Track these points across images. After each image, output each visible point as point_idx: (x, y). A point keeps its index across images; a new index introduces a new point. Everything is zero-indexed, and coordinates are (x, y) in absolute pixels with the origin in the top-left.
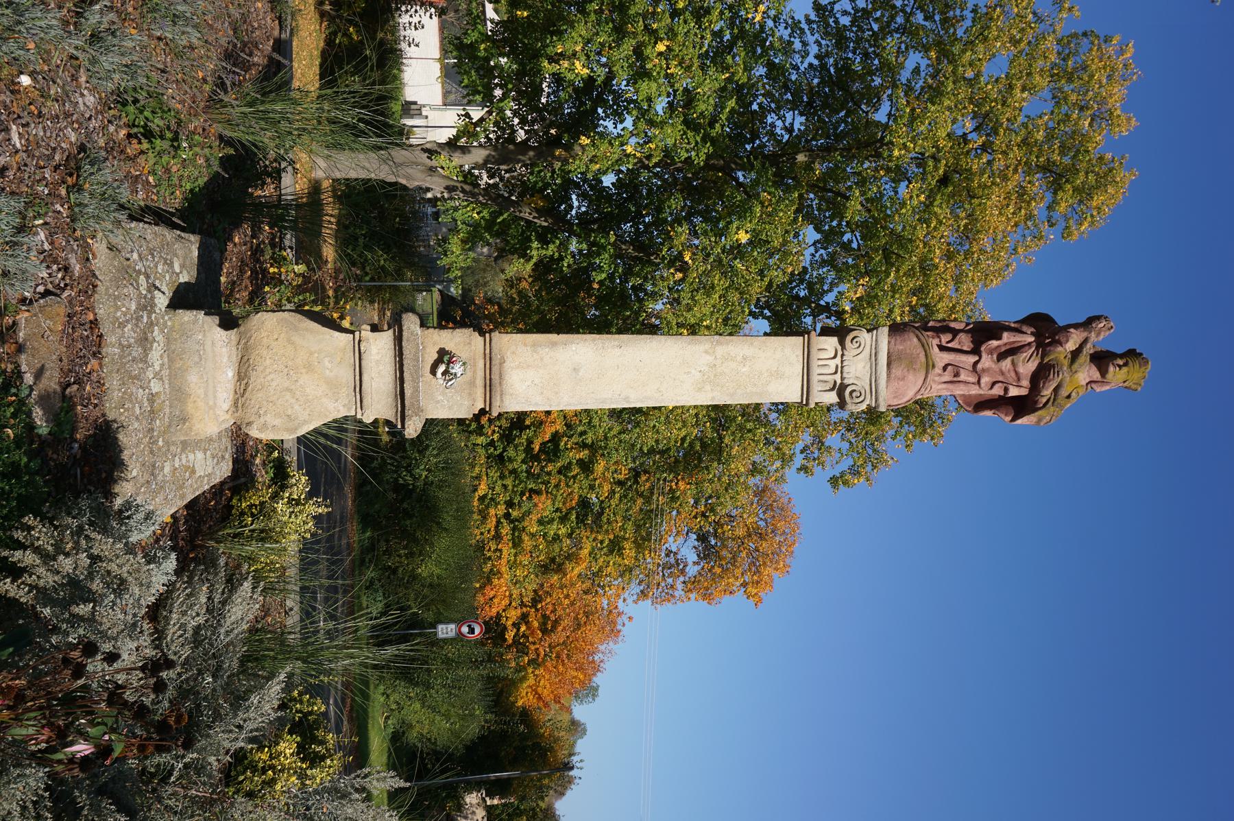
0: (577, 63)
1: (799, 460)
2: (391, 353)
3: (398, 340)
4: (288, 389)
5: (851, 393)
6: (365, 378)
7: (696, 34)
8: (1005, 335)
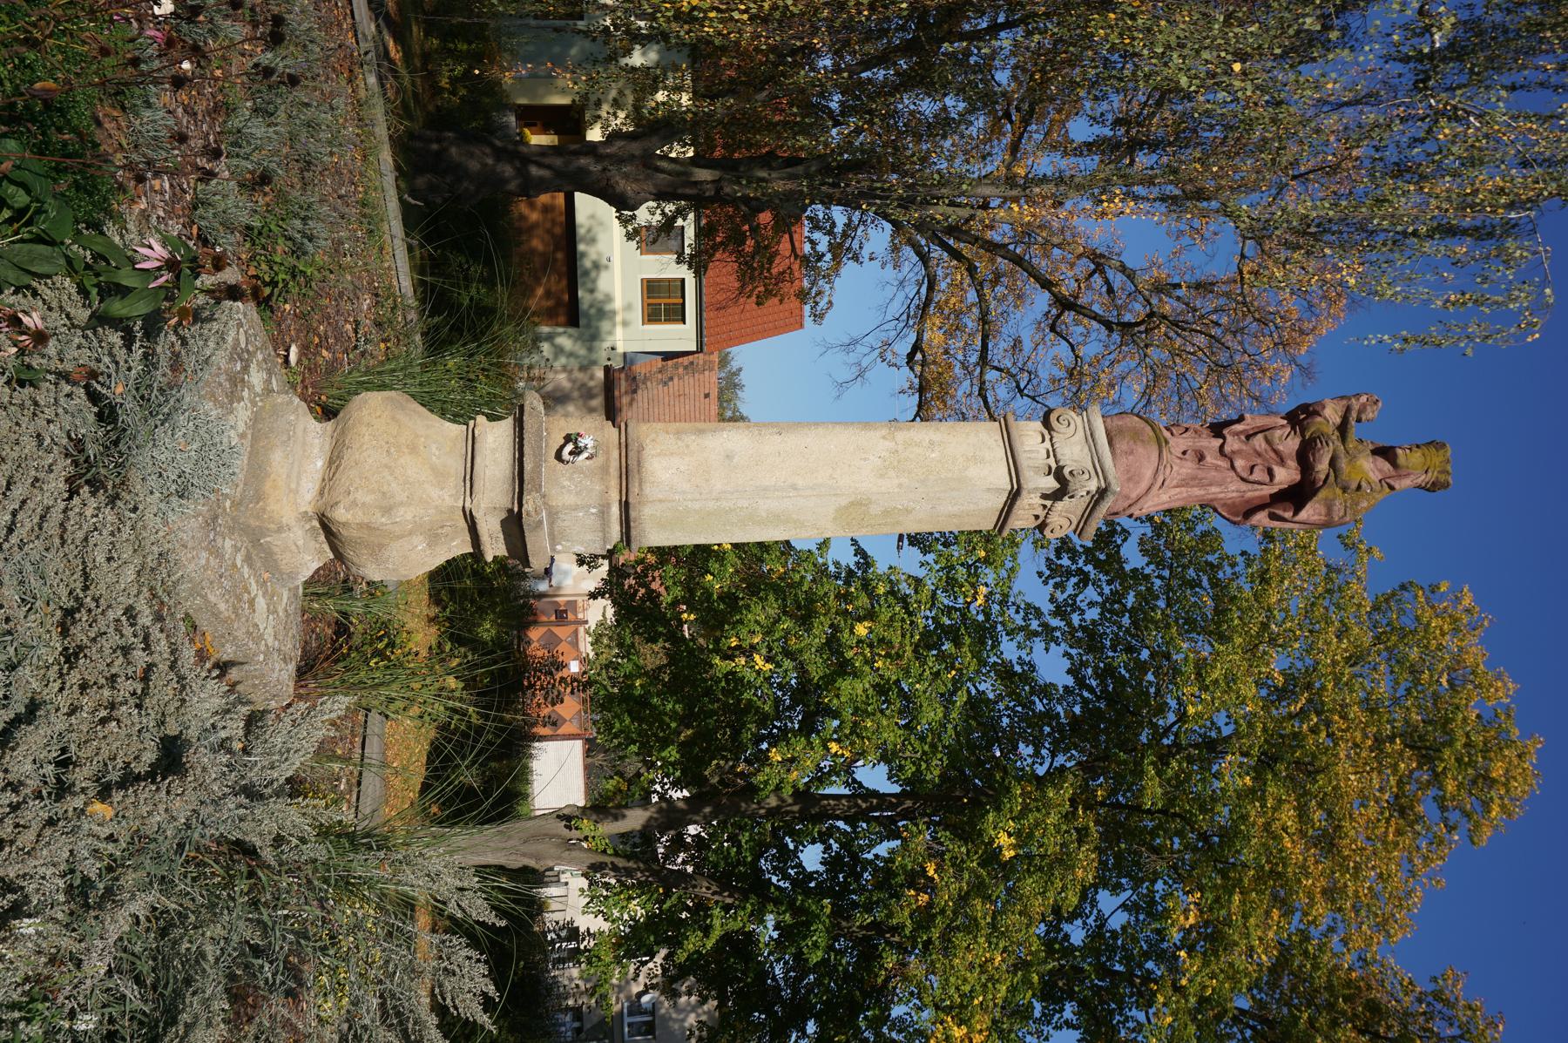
0: (757, 657)
2: (511, 439)
3: (519, 424)
4: (386, 466)
6: (478, 460)
7: (903, 620)
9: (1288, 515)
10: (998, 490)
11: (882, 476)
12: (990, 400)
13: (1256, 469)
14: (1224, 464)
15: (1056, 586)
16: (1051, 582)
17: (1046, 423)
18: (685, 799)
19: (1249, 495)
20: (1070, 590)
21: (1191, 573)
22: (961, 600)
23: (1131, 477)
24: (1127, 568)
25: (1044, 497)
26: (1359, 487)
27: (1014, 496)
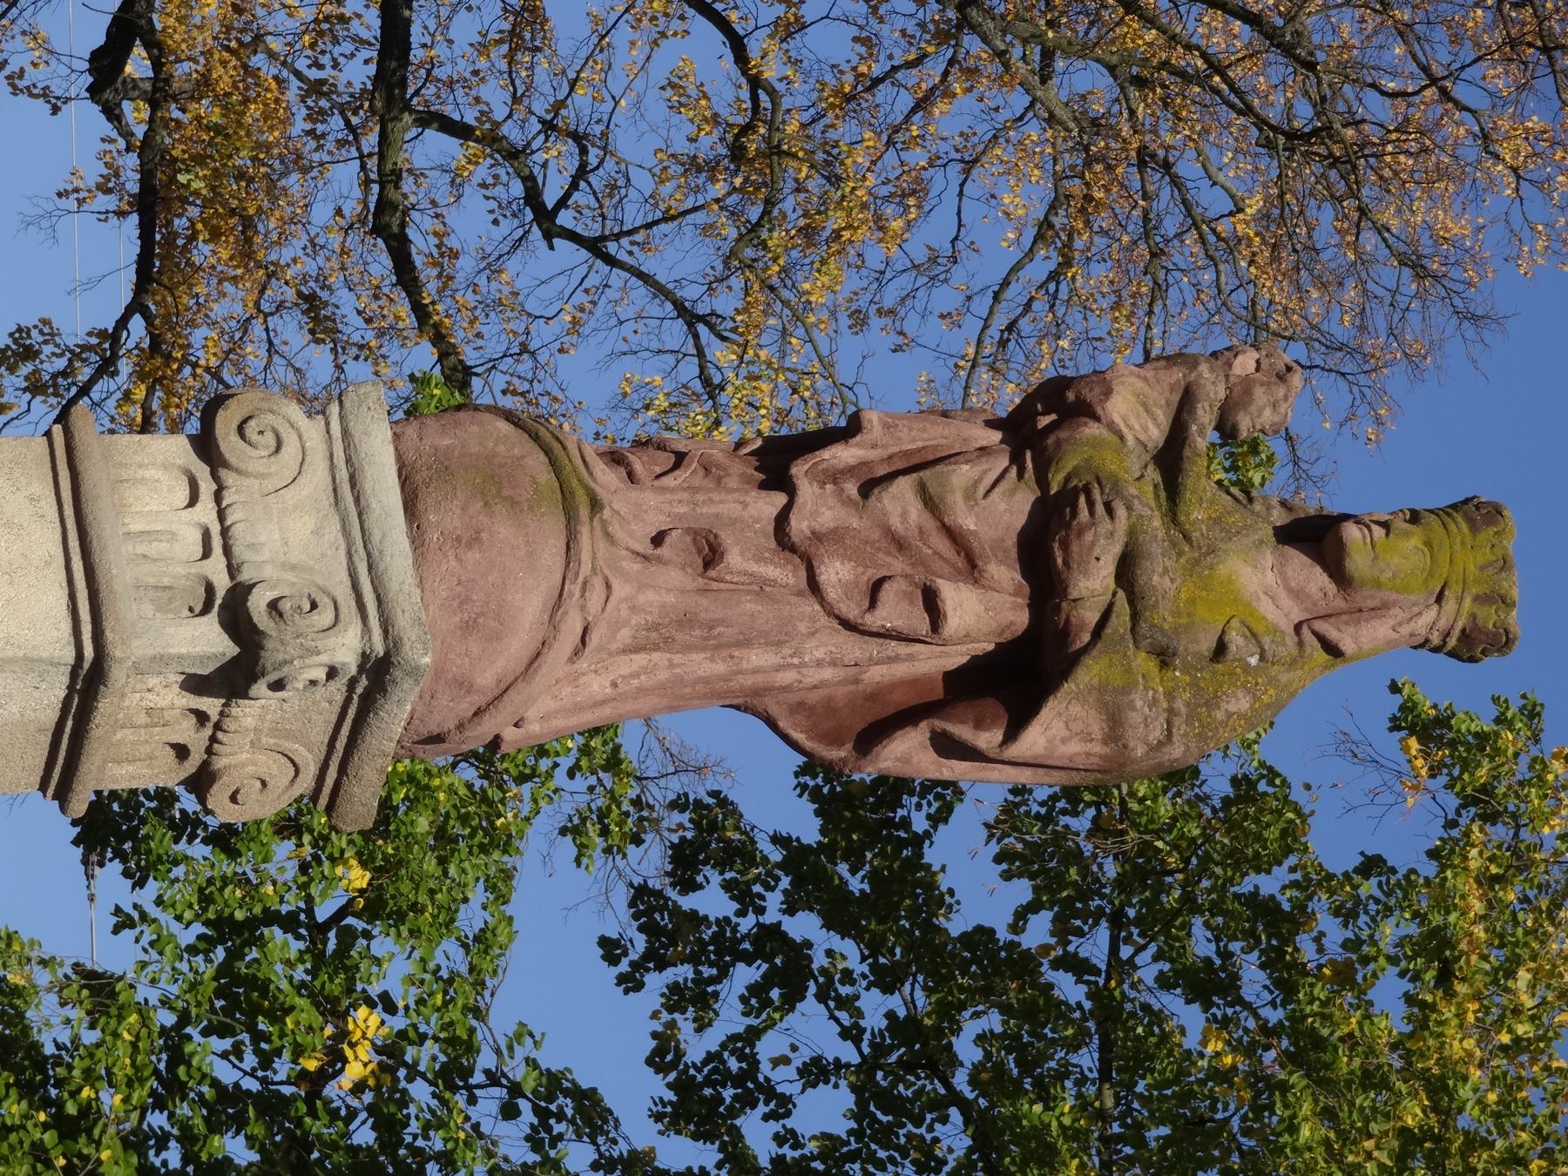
9: (988, 739)
10: (31, 663)
12: (421, 244)
13: (888, 593)
14: (786, 574)
15: (677, 998)
16: (656, 982)
17: (205, 446)
19: (877, 674)
20: (730, 1018)
21: (1201, 945)
22: (283, 1068)
23: (476, 620)
24: (956, 926)
25: (195, 684)
26: (1220, 649)
27: (88, 682)
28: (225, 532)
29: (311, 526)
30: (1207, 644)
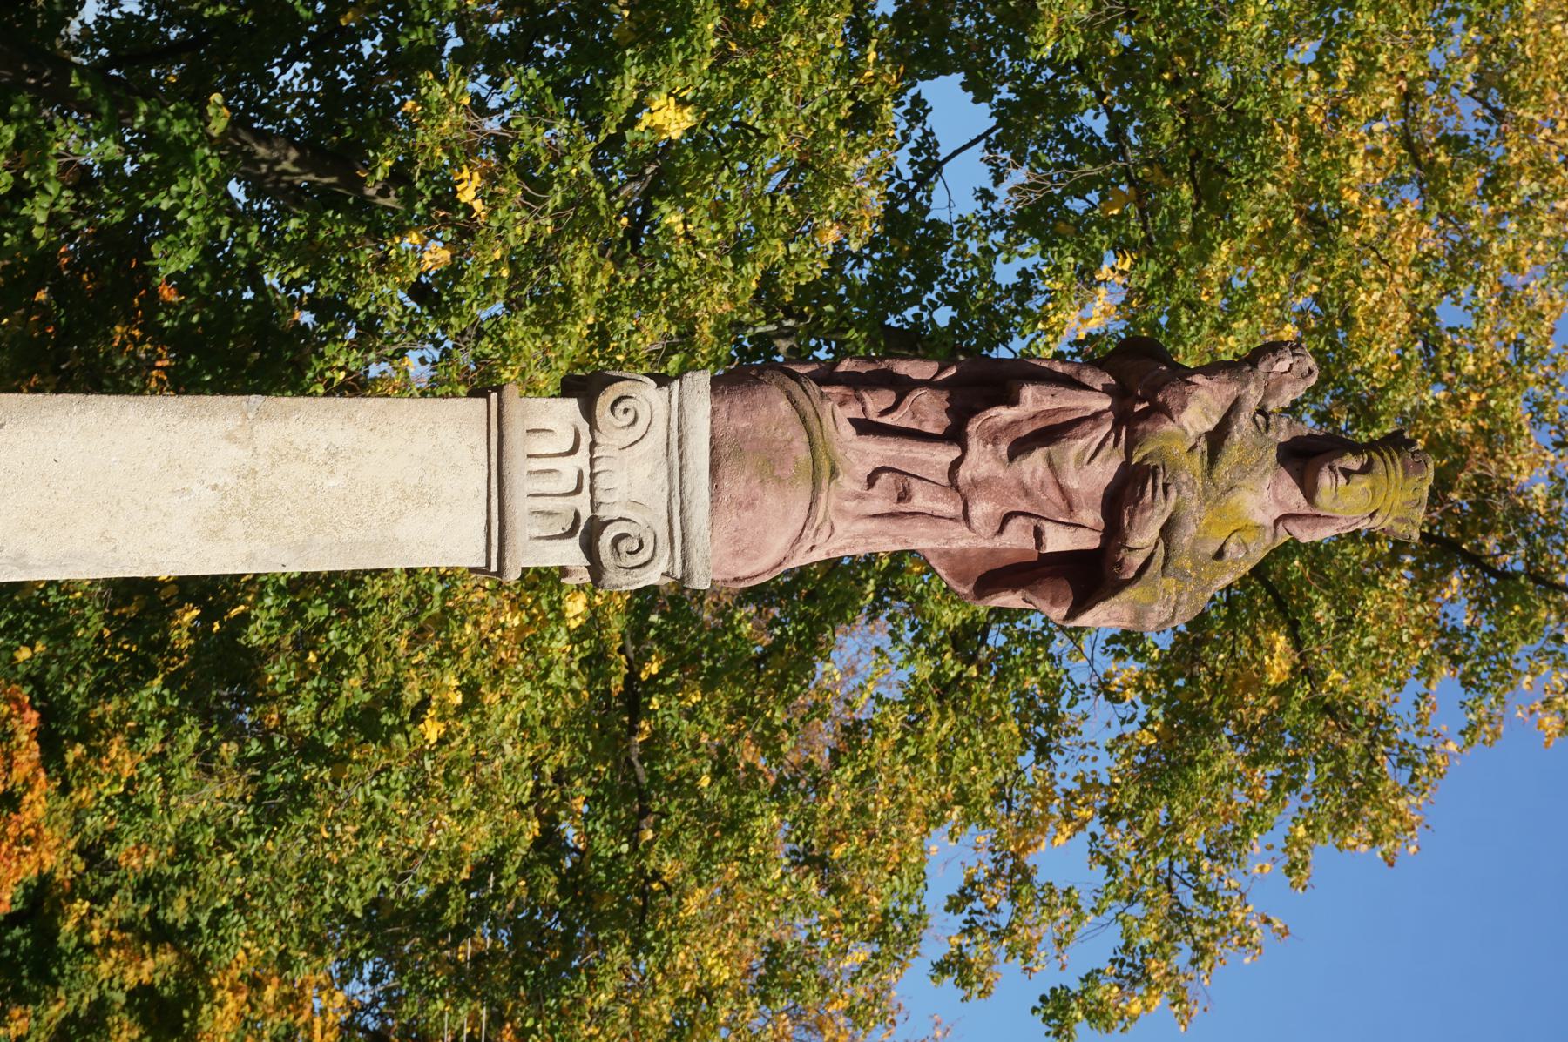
1: (942, 934)
5: (616, 542)
8: (1028, 392)
11: (214, 535)
18: (198, 618)
26: (1220, 554)
28: (593, 476)
29: (648, 472)
30: (1213, 548)
